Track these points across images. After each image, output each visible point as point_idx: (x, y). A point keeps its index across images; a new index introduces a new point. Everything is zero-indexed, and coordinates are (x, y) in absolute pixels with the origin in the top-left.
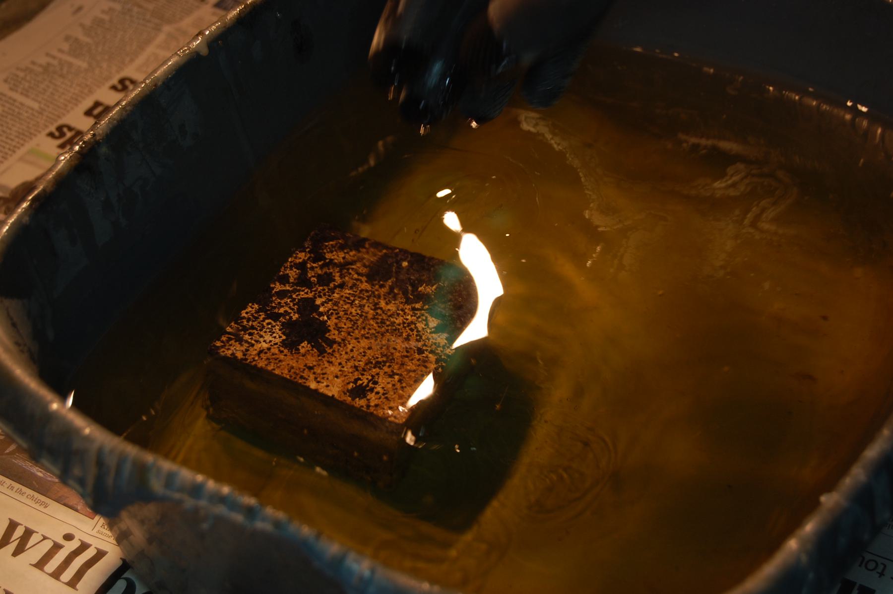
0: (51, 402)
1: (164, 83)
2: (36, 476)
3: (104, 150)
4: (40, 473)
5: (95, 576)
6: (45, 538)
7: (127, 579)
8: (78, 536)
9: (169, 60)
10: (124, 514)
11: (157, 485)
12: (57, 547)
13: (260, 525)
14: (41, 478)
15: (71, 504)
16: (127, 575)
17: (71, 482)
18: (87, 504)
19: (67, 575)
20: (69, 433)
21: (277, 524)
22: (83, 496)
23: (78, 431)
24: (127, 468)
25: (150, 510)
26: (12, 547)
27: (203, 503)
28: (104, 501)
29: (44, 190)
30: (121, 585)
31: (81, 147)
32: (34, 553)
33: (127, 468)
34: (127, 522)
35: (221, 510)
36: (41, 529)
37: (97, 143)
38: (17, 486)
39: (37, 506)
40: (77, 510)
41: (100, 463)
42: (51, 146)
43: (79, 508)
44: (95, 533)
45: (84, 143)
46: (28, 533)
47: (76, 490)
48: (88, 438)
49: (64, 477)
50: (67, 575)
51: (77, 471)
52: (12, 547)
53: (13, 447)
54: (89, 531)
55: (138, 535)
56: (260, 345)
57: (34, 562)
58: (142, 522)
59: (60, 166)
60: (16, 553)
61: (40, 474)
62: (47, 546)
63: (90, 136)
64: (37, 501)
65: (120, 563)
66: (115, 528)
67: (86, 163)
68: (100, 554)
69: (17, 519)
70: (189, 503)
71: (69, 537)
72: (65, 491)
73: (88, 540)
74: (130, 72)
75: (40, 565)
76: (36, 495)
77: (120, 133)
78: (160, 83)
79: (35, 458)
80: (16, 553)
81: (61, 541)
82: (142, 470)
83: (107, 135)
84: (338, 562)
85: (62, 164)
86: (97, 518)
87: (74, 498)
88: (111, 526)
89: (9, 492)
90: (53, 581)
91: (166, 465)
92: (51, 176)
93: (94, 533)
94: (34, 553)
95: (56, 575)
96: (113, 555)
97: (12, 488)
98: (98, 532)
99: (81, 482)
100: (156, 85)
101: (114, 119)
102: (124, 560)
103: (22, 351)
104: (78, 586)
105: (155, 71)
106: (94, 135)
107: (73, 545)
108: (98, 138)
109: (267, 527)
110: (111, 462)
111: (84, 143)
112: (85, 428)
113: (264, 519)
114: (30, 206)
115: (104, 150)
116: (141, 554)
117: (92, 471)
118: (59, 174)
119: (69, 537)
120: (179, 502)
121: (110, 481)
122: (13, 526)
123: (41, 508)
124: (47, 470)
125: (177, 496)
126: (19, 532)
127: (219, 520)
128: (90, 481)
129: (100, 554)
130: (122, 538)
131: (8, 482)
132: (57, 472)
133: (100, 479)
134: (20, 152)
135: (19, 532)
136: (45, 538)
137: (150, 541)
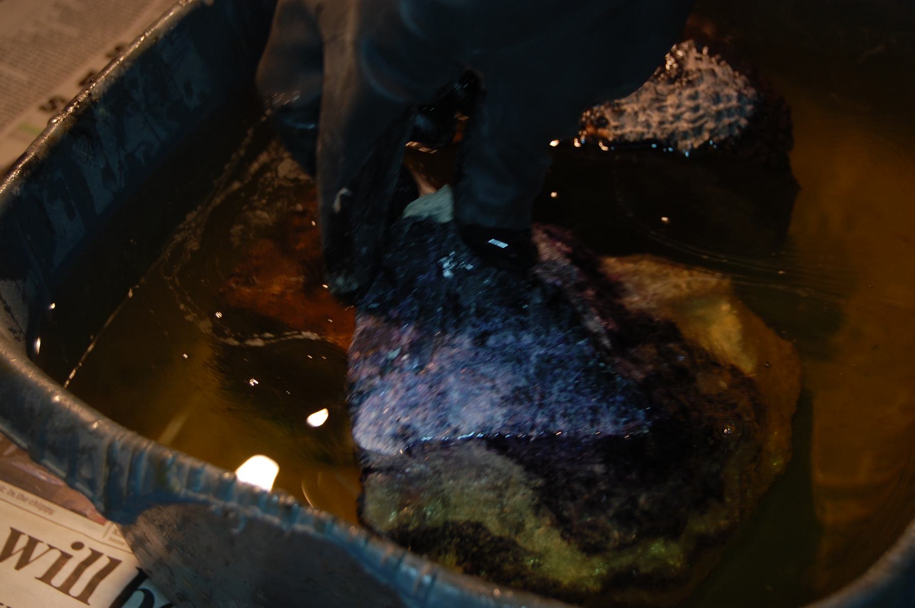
0: (53, 394)
1: (165, 36)
2: (39, 480)
3: (101, 111)
4: (43, 476)
5: (109, 589)
6: (51, 547)
7: (144, 591)
8: (88, 544)
9: (170, 11)
10: (141, 520)
11: (178, 485)
12: (65, 557)
13: (299, 527)
14: (43, 481)
15: (78, 508)
16: (144, 586)
17: (78, 485)
18: (98, 509)
19: (78, 588)
20: (75, 427)
21: (320, 525)
22: (92, 500)
23: (85, 426)
24: (143, 465)
25: (170, 513)
26: (15, 559)
27: (232, 504)
28: (116, 506)
29: (36, 157)
30: (138, 597)
31: (76, 108)
32: (40, 566)
33: (143, 465)
34: (143, 527)
35: (257, 512)
36: (46, 538)
37: (94, 103)
38: (18, 491)
39: (41, 513)
40: (85, 516)
41: (111, 461)
42: (39, 120)
43: (88, 513)
44: (107, 540)
45: (79, 103)
46: (33, 543)
47: (83, 493)
48: (95, 433)
49: (71, 479)
50: (78, 588)
51: (85, 472)
52: (15, 559)
53: (12, 448)
54: (100, 539)
55: (156, 541)
56: (702, 95)
57: (40, 575)
58: (161, 527)
59: (53, 130)
60: (19, 567)
61: (43, 478)
62: (55, 556)
63: (85, 96)
64: (41, 507)
65: (135, 573)
66: (130, 535)
67: (82, 124)
68: (114, 563)
69: (18, 528)
70: (217, 505)
71: (78, 546)
72: (72, 494)
73: (99, 548)
74: (126, 37)
75: (47, 578)
76: (40, 500)
77: (119, 91)
78: (161, 36)
79: (37, 459)
80: (19, 567)
81: (70, 551)
82: (160, 467)
83: (104, 94)
84: (391, 569)
85: (54, 128)
86: (109, 523)
87: (90, 508)
88: (124, 533)
89: (9, 498)
90: (61, 595)
91: (189, 462)
92: (43, 141)
93: (106, 540)
94: (40, 566)
95: (65, 588)
96: (128, 564)
97: (13, 494)
98: (111, 539)
99: (91, 484)
100: (156, 38)
101: (112, 77)
102: (140, 570)
103: (17, 339)
104: (90, 600)
105: (155, 23)
106: (90, 94)
107: (84, 554)
108: (94, 98)
109: (310, 529)
110: (124, 460)
111: (79, 103)
112: (93, 422)
113: (304, 521)
114: (21, 174)
115: (101, 111)
116: (160, 563)
117: (104, 470)
118: (52, 139)
119: (78, 546)
120: (206, 504)
121: (124, 482)
122: (15, 535)
123: (46, 515)
124: (51, 472)
125: (202, 497)
126: (22, 542)
127: (252, 522)
128: (101, 483)
129: (114, 563)
130: (137, 545)
131: (8, 487)
132: (63, 474)
133: (112, 480)
134: (10, 128)
135: (22, 542)
136: (51, 547)
137: (169, 548)
